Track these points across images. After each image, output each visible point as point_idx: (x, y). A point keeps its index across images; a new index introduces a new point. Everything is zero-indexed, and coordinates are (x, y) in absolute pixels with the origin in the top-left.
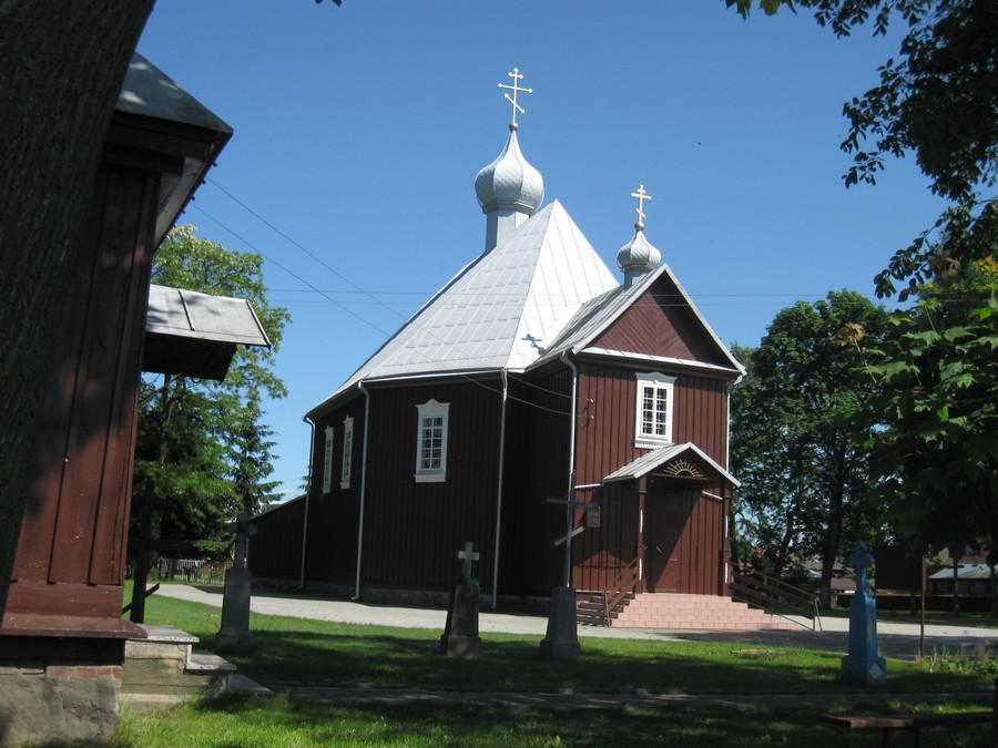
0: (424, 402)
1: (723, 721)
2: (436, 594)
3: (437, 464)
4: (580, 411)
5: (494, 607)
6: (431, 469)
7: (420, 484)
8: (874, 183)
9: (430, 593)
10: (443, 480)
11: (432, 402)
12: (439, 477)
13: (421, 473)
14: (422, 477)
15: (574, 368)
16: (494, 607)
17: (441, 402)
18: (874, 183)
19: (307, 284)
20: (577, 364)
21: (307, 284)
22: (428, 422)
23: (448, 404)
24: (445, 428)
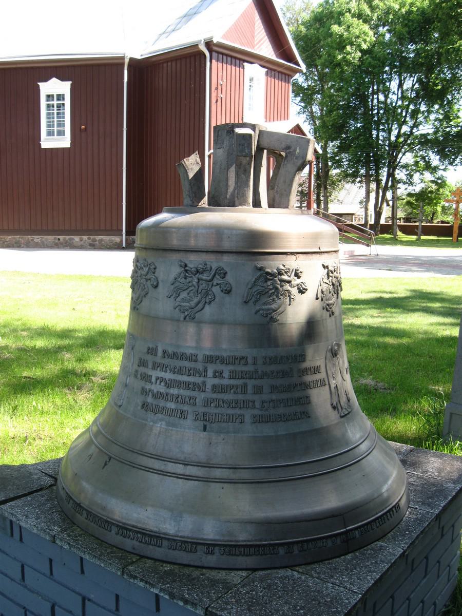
0: (46, 80)
1: (102, 448)
2: (67, 237)
3: (61, 133)
4: (270, 477)
5: (124, 246)
6: (55, 136)
7: (46, 149)
8: (323, 265)
9: (61, 238)
10: (69, 146)
11: (54, 80)
12: (65, 142)
13: (46, 140)
14: (47, 142)
15: (207, 54)
16: (124, 246)
17: (62, 80)
18: (323, 265)
19: (421, 562)
20: (211, 51)
21: (421, 562)
22: (49, 97)
23: (70, 83)
24: (67, 102)
